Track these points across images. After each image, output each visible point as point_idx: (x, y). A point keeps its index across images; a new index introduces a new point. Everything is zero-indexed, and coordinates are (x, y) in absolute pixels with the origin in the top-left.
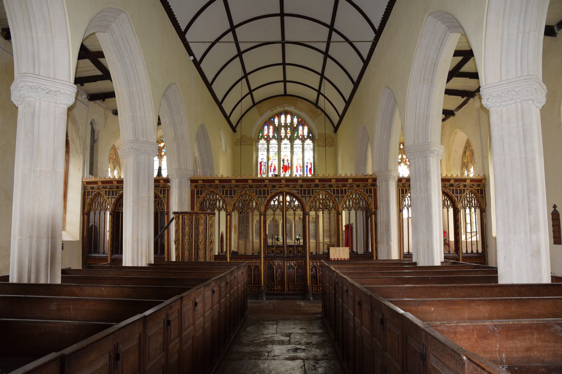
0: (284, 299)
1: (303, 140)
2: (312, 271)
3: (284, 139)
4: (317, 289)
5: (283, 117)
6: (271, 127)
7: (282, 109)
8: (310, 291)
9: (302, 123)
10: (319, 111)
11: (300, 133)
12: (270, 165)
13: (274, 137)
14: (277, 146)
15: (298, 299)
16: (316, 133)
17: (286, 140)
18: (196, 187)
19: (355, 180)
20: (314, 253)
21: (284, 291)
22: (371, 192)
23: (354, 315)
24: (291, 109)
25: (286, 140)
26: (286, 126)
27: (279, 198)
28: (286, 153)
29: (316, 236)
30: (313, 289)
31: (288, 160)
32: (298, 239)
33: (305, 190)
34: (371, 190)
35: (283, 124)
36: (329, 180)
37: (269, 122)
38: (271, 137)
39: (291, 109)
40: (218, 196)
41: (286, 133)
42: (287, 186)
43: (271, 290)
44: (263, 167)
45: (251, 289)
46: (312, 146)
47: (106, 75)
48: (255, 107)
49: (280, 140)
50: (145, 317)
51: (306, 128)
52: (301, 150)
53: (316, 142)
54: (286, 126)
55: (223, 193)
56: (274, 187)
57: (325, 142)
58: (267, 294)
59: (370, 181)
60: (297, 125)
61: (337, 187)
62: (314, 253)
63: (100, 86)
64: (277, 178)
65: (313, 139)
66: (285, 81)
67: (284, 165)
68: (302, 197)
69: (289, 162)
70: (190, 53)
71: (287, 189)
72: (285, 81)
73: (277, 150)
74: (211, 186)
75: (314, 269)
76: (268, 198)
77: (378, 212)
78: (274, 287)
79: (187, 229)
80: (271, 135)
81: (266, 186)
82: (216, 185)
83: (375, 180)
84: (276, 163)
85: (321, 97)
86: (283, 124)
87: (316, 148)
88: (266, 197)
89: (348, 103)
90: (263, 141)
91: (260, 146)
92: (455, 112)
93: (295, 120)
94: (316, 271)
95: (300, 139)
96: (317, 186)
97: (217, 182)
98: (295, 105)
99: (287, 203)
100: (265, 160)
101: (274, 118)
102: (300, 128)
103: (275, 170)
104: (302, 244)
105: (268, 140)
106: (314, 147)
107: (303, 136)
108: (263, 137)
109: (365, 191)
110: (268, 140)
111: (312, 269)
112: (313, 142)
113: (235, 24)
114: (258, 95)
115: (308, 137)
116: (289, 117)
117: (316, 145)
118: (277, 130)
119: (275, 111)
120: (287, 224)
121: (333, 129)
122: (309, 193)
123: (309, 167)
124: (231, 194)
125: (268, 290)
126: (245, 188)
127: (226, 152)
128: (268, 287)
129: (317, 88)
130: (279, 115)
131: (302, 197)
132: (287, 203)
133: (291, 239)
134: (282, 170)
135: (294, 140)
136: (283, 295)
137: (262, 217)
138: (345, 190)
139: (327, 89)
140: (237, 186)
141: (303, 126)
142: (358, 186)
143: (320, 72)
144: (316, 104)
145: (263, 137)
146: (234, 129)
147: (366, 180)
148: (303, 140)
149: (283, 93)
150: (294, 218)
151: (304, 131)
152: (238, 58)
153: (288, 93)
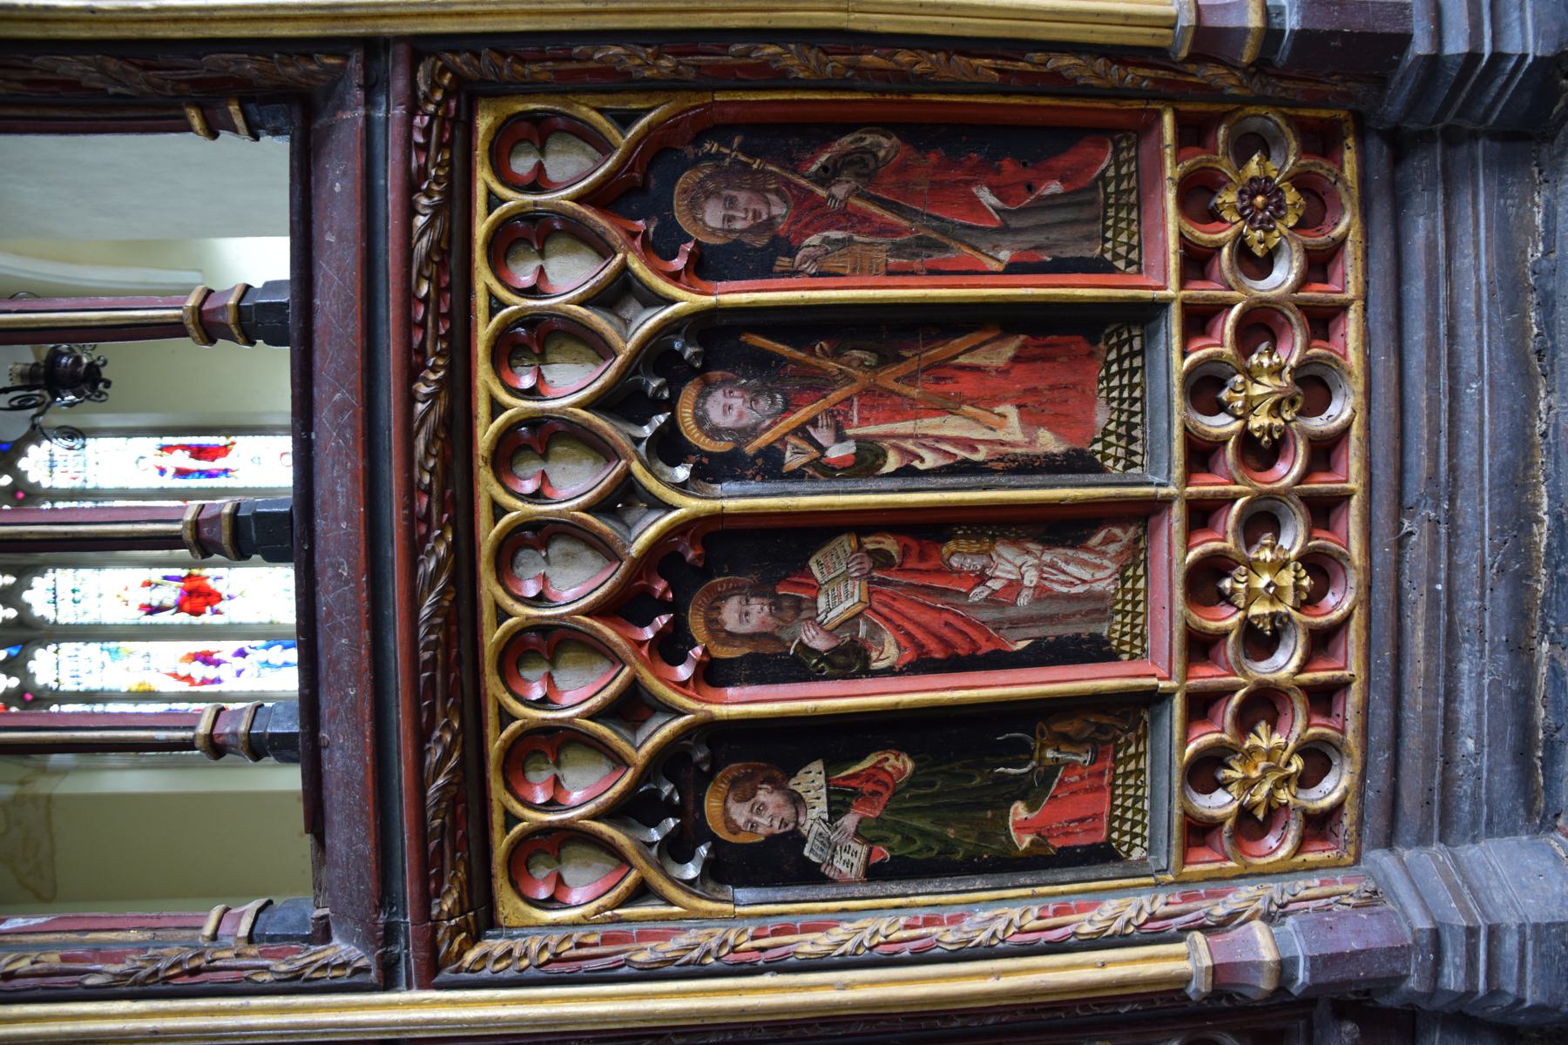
2: (780, 863)
3: (24, 608)
12: (184, 687)
14: (66, 647)
17: (27, 596)
25: (27, 596)
31: (148, 584)
38: (14, 682)
46: (58, 446)
50: (812, 192)
67: (180, 608)
73: (94, 647)
75: (753, 815)
84: (171, 653)
92: (188, 536)
94: (776, 747)
103: (206, 659)
123: (184, 460)
134: (207, 618)
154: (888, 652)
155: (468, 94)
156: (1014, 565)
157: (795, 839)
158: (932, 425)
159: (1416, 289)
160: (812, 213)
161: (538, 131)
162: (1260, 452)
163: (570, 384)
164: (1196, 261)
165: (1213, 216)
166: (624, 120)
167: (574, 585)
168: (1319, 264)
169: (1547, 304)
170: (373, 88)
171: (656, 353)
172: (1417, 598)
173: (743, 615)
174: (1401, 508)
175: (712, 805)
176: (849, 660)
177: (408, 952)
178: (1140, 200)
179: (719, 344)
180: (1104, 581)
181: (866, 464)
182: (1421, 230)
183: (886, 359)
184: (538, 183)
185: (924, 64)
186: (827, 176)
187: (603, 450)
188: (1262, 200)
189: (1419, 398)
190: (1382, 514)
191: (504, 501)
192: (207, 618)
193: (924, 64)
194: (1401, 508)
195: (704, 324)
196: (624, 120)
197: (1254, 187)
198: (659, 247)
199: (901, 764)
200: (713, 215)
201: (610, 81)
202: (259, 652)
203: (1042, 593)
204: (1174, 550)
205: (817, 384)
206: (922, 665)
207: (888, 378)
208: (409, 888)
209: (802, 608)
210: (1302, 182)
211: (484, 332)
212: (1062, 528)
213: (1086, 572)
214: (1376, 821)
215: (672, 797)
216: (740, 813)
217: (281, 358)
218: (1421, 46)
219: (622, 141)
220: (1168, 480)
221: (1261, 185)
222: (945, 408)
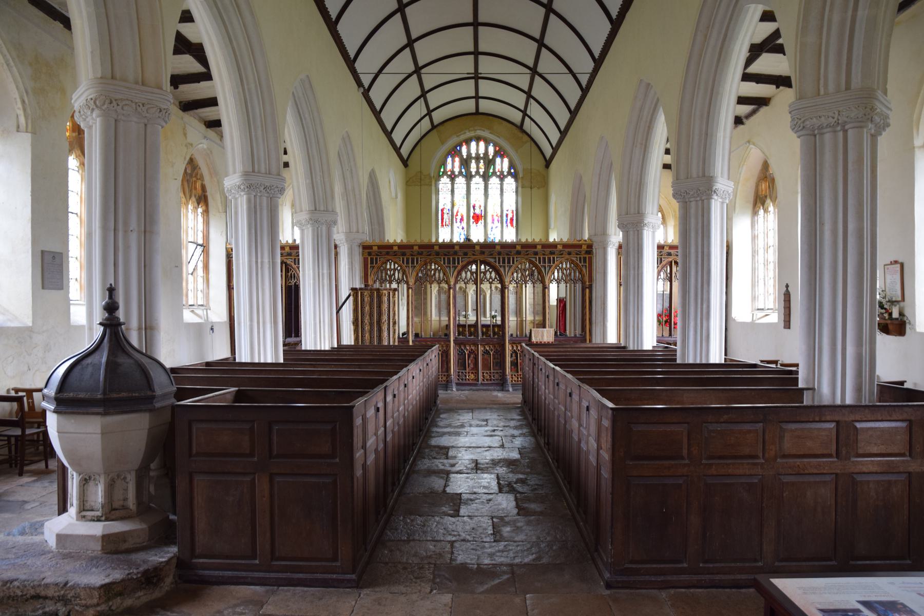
1: (502, 178)
3: (474, 176)
5: (473, 144)
6: (457, 159)
7: (472, 134)
9: (500, 153)
10: (526, 137)
11: (498, 167)
13: (460, 173)
14: (465, 186)
15: (494, 390)
16: (520, 168)
18: (370, 254)
19: (565, 246)
20: (515, 335)
22: (585, 261)
23: (599, 448)
24: (486, 134)
26: (478, 158)
28: (477, 197)
29: (519, 311)
32: (494, 317)
34: (585, 258)
35: (474, 155)
37: (454, 152)
39: (486, 134)
41: (478, 168)
42: (483, 253)
44: (445, 216)
47: (207, 76)
48: (435, 131)
49: (469, 177)
51: (506, 160)
52: (499, 192)
53: (520, 181)
54: (478, 158)
56: (466, 254)
57: (534, 179)
58: (457, 384)
59: (584, 247)
62: (515, 335)
63: (198, 90)
65: (515, 176)
66: (477, 97)
69: (482, 208)
70: (359, 83)
71: (482, 257)
72: (477, 97)
74: (388, 254)
76: (459, 268)
77: (594, 286)
79: (367, 308)
80: (457, 170)
81: (456, 253)
83: (590, 246)
84: (463, 211)
85: (527, 118)
86: (474, 155)
87: (520, 189)
88: (456, 267)
89: (563, 133)
90: (445, 180)
91: (441, 186)
92: (744, 120)
93: (491, 150)
95: (497, 176)
96: (518, 253)
97: (396, 248)
98: (490, 129)
100: (449, 206)
101: (461, 145)
102: (498, 160)
103: (462, 220)
104: (499, 323)
105: (452, 178)
106: (517, 188)
107: (502, 172)
108: (445, 173)
109: (581, 259)
110: (452, 178)
112: (516, 180)
113: (431, 108)
114: (438, 116)
115: (509, 173)
116: (482, 144)
117: (520, 185)
118: (465, 163)
119: (463, 137)
120: (481, 301)
121: (543, 163)
123: (510, 216)
124: (413, 263)
127: (397, 197)
129: (526, 89)
130: (468, 142)
133: (485, 316)
134: (472, 220)
135: (489, 177)
136: (475, 385)
139: (535, 110)
140: (421, 254)
141: (502, 157)
142: (569, 254)
143: (522, 108)
144: (521, 127)
145: (445, 173)
146: (405, 163)
147: (580, 246)
148: (502, 178)
149: (474, 111)
150: (490, 291)
151: (502, 164)
152: (408, 50)
153: (481, 110)
192: (472, 220)
202: (464, 232)
215: (515, 352)
217: (34, 394)
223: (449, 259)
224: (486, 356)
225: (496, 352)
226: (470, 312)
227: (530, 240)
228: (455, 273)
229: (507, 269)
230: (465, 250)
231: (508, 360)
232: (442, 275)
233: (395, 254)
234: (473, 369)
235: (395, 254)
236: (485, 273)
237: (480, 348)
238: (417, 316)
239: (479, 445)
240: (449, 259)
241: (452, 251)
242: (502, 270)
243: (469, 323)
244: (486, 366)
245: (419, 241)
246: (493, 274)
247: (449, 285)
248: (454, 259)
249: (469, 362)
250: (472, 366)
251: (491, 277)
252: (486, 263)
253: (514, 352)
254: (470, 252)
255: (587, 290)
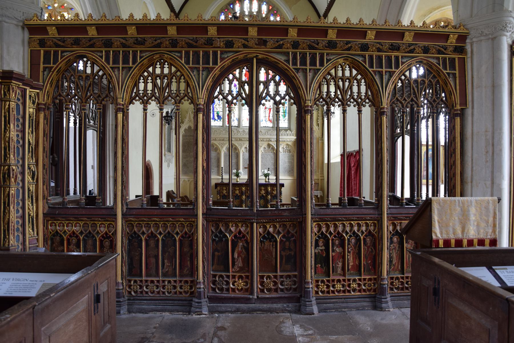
0: (251, 311)
2: (317, 245)
4: (328, 287)
8: (312, 294)
15: (283, 311)
18: (42, 43)
21: (252, 293)
22: (453, 67)
27: (241, 73)
30: (317, 286)
32: (266, 175)
33: (304, 57)
34: (452, 61)
35: (247, 13)
36: (362, 33)
40: (96, 68)
42: (264, 43)
43: (221, 290)
45: (175, 287)
55: (107, 60)
58: (212, 299)
59: (453, 40)
60: (266, 15)
61: (379, 50)
64: (238, 22)
68: (298, 70)
74: (77, 42)
75: (321, 243)
76: (217, 71)
77: (469, 111)
78: (228, 283)
81: (210, 42)
82: (91, 39)
83: (462, 38)
86: (247, 13)
88: (209, 70)
96: (332, 45)
99: (261, 87)
101: (234, 3)
111: (317, 242)
122: (313, 63)
124: (126, 61)
125: (214, 290)
126: (159, 46)
128: (214, 282)
131: (298, 70)
132: (261, 87)
136: (247, 301)
137: (200, 116)
138: (397, 58)
142: (426, 50)
150: (276, 118)
154: (334, 254)
155: (378, 221)
156: (340, 264)
157: (319, 246)
158: (352, 257)
159: (363, 299)
160: (368, 247)
161: (375, 225)
162: (349, 286)
163: (356, 229)
164: (365, 279)
165: (368, 281)
166: (376, 233)
167: (340, 229)
168: (364, 291)
169: (362, 310)
170: (379, 214)
171: (358, 235)
172: (337, 300)
173: (337, 242)
174: (344, 298)
175: (322, 240)
176: (333, 251)
177: (314, 216)
178: (369, 275)
179: (358, 240)
180: (339, 272)
181: (349, 252)
182: (368, 299)
183: (357, 254)
184: (371, 226)
185: (380, 257)
186: (371, 249)
187: (350, 231)
188: (370, 285)
189: (354, 300)
190: (344, 297)
191: (347, 223)
193: (380, 257)
194: (344, 298)
195: (360, 239)
196: (376, 233)
197: (371, 284)
198: (366, 236)
199: (324, 255)
200: (368, 240)
201: (379, 232)
203: (338, 267)
204: (341, 278)
205: (355, 248)
206: (332, 257)
207: (355, 254)
208: (319, 217)
209: (337, 247)
210: (371, 289)
211: (360, 222)
212: (343, 268)
213: (339, 270)
214: (318, 298)
215: (323, 236)
216: (321, 242)
218: (383, 297)
219: (374, 233)
220: (347, 278)
221: (371, 285)
222: (353, 258)
223: (196, 55)
224: (267, 243)
225: (287, 236)
226: (241, 170)
227: (354, 21)
228: (209, 82)
229: (310, 76)
230: (230, 37)
231: (310, 252)
232: (183, 86)
233: (91, 44)
234: (241, 270)
235: (91, 44)
236: (266, 84)
237: (257, 230)
238: (185, 173)
239: (251, 297)
240: (196, 55)
241: (202, 38)
242: (300, 76)
243: (240, 181)
244: (267, 265)
245: (138, 16)
246: (283, 88)
247: (196, 105)
248: (206, 55)
249: (235, 256)
250: (240, 263)
251: (277, 93)
252: (270, 65)
253: (322, 238)
254: (238, 40)
255: (458, 120)
